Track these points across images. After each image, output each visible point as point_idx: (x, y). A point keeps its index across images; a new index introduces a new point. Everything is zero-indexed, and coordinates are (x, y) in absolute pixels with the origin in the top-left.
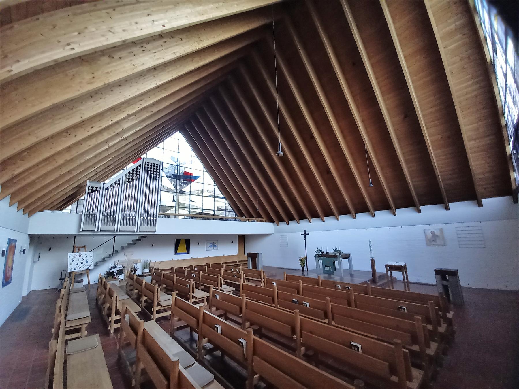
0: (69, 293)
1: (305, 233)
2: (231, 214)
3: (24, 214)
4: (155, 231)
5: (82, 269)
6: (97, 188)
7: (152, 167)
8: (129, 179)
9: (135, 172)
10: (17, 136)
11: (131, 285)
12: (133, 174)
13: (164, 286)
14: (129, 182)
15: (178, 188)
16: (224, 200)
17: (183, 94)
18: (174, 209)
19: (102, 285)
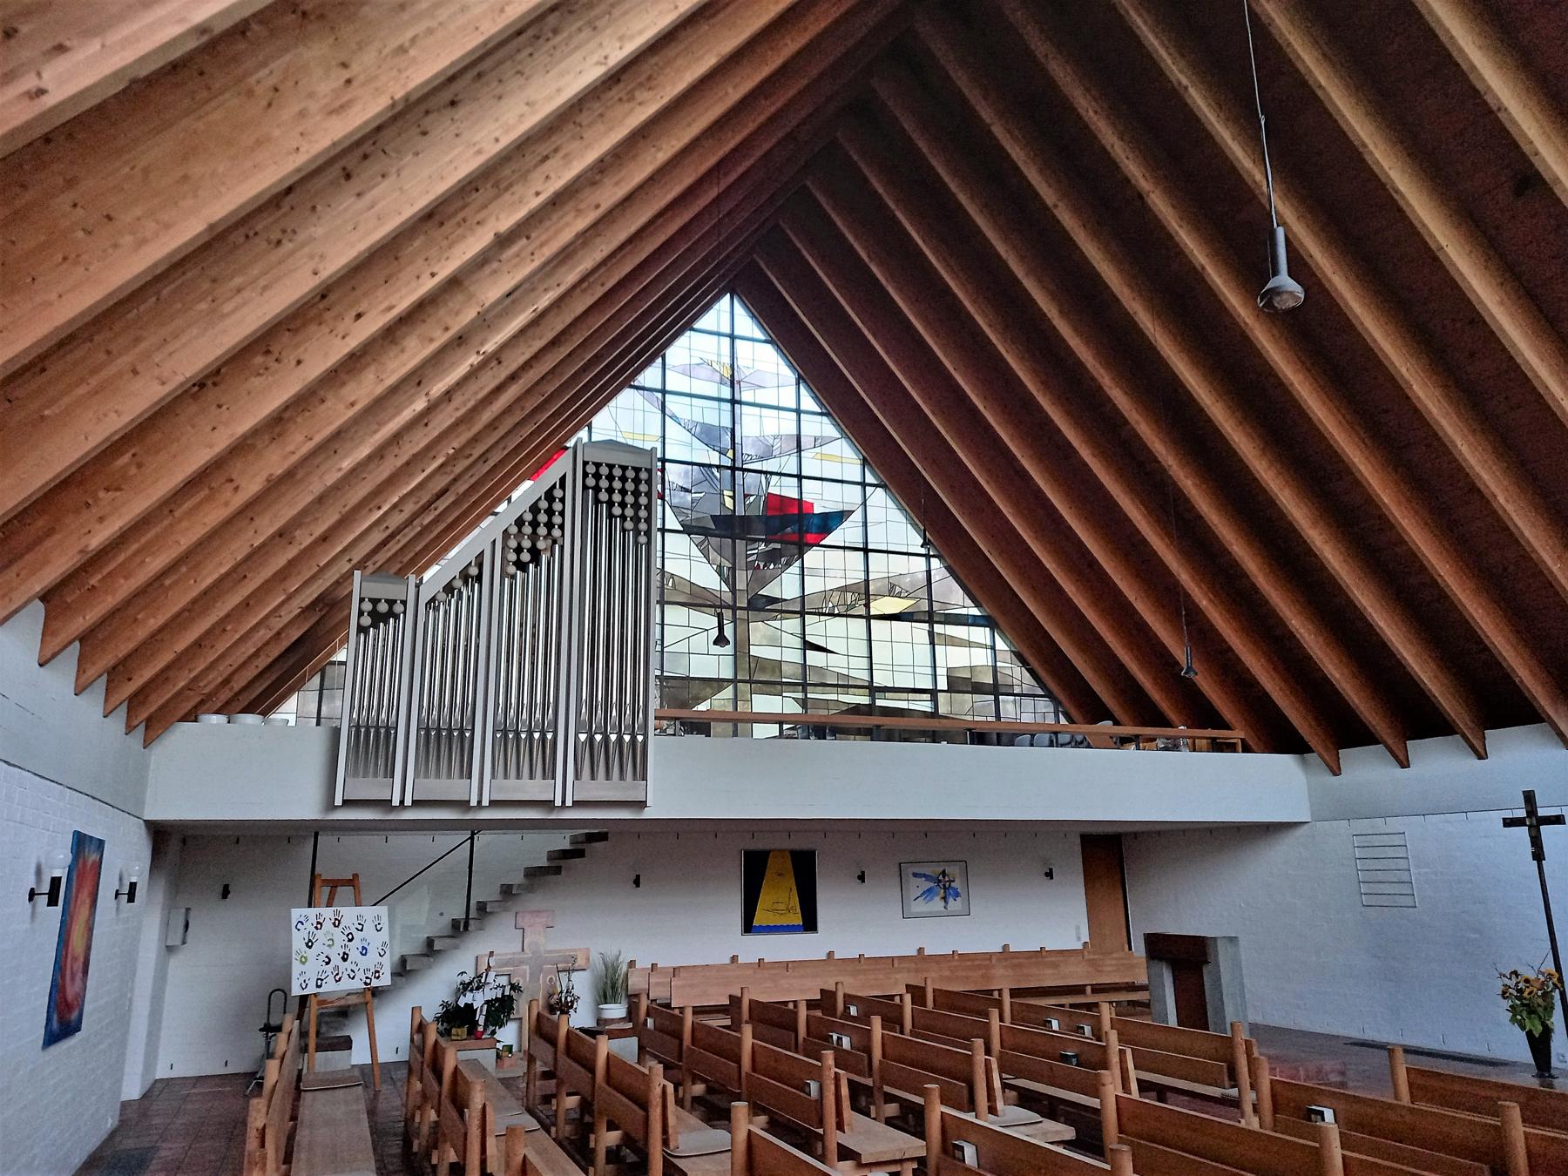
0: (298, 1090)
1: (1532, 811)
2: (1033, 711)
3: (130, 729)
4: (642, 804)
5: (347, 985)
6: (391, 603)
7: (617, 484)
8: (519, 550)
9: (543, 518)
10: (94, 382)
11: (547, 1075)
12: (535, 524)
13: (699, 1089)
14: (522, 566)
15: (741, 585)
16: (981, 634)
17: (732, 93)
18: (728, 692)
19: (425, 1058)
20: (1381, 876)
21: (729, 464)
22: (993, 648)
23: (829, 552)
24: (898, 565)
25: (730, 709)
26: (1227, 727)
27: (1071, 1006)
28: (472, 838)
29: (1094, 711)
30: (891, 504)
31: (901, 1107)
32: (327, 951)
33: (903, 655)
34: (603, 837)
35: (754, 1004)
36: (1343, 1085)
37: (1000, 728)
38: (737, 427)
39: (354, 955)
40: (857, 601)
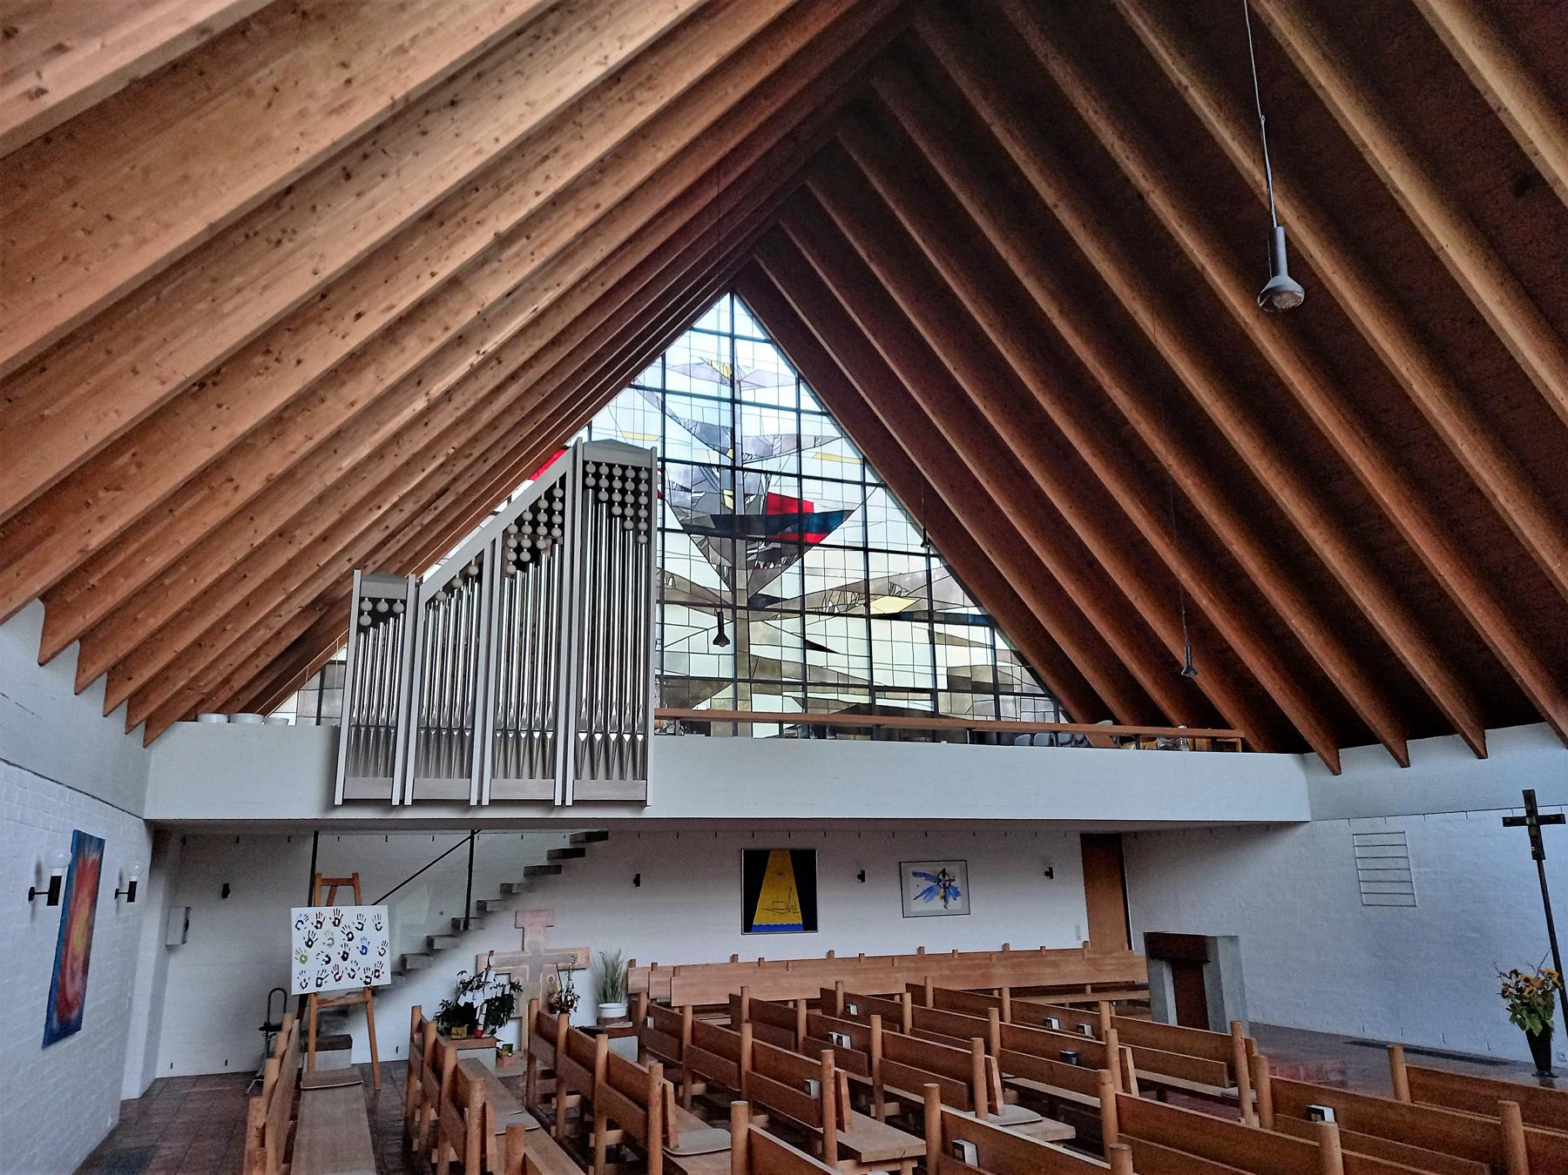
0: (298, 1089)
1: (1532, 811)
2: (1033, 710)
3: (130, 728)
4: (642, 804)
5: (347, 984)
6: (391, 602)
7: (617, 484)
8: (519, 550)
9: (543, 517)
10: (94, 381)
11: (547, 1075)
12: (535, 524)
13: (699, 1088)
14: (522, 566)
15: (741, 585)
16: (981, 634)
17: (732, 93)
18: (728, 692)
19: (425, 1058)
20: (1381, 875)
21: (729, 463)
22: (993, 647)
23: (829, 552)
24: (898, 564)
25: (730, 708)
26: (1227, 726)
27: (1071, 1005)
28: (472, 838)
29: (1094, 710)
30: (891, 503)
31: (901, 1106)
32: (327, 950)
33: (903, 654)
34: (603, 836)
35: (754, 1003)
36: (1343, 1084)
37: (1000, 727)
38: (737, 427)
39: (354, 954)
40: (857, 600)
